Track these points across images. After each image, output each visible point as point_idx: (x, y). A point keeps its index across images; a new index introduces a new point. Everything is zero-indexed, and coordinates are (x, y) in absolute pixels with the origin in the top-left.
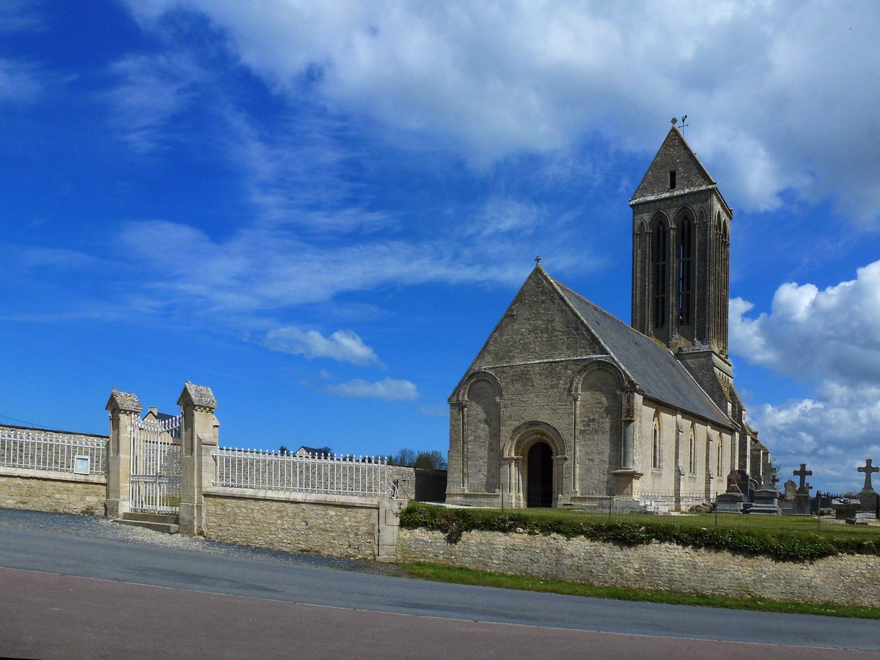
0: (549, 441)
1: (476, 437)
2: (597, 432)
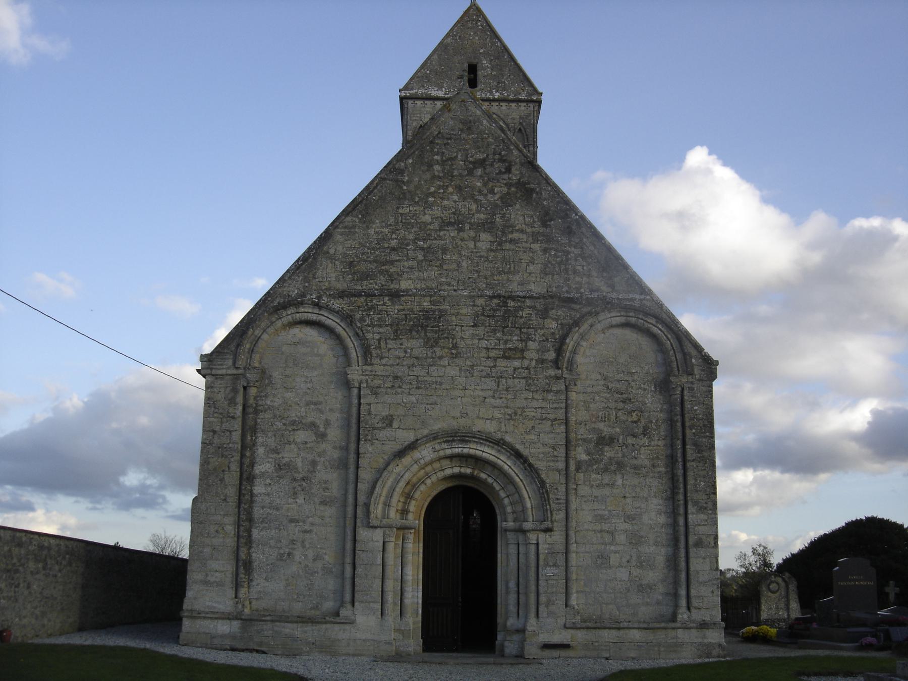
0: (495, 484)
1: (279, 467)
2: (620, 466)
